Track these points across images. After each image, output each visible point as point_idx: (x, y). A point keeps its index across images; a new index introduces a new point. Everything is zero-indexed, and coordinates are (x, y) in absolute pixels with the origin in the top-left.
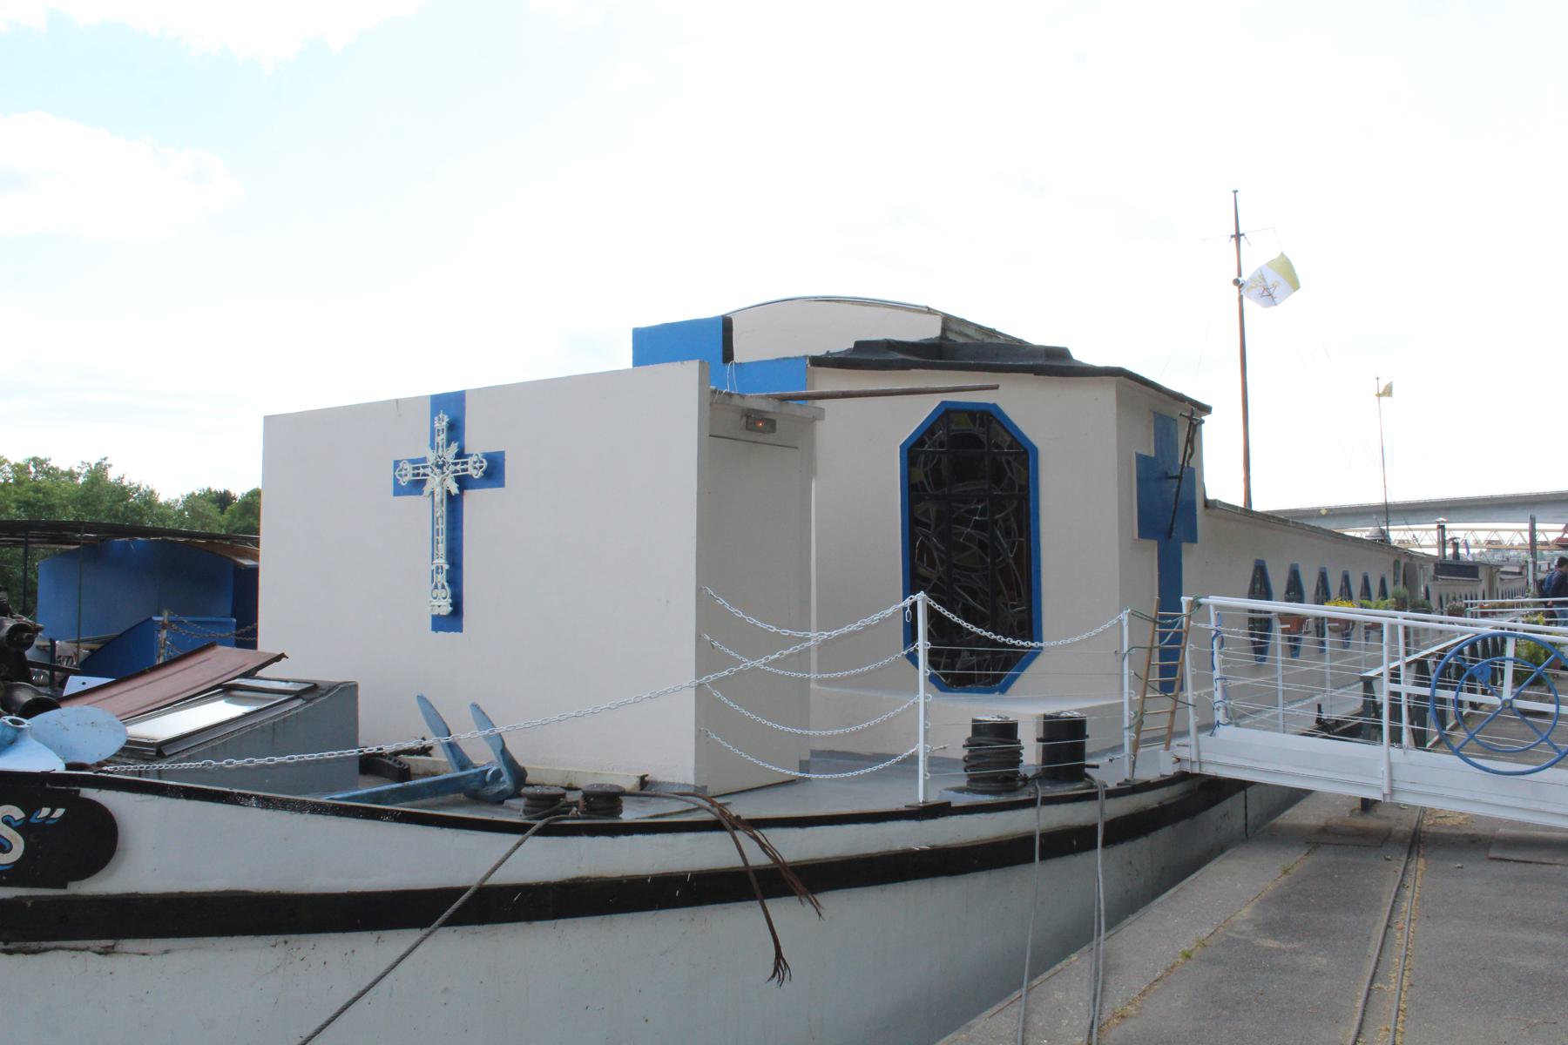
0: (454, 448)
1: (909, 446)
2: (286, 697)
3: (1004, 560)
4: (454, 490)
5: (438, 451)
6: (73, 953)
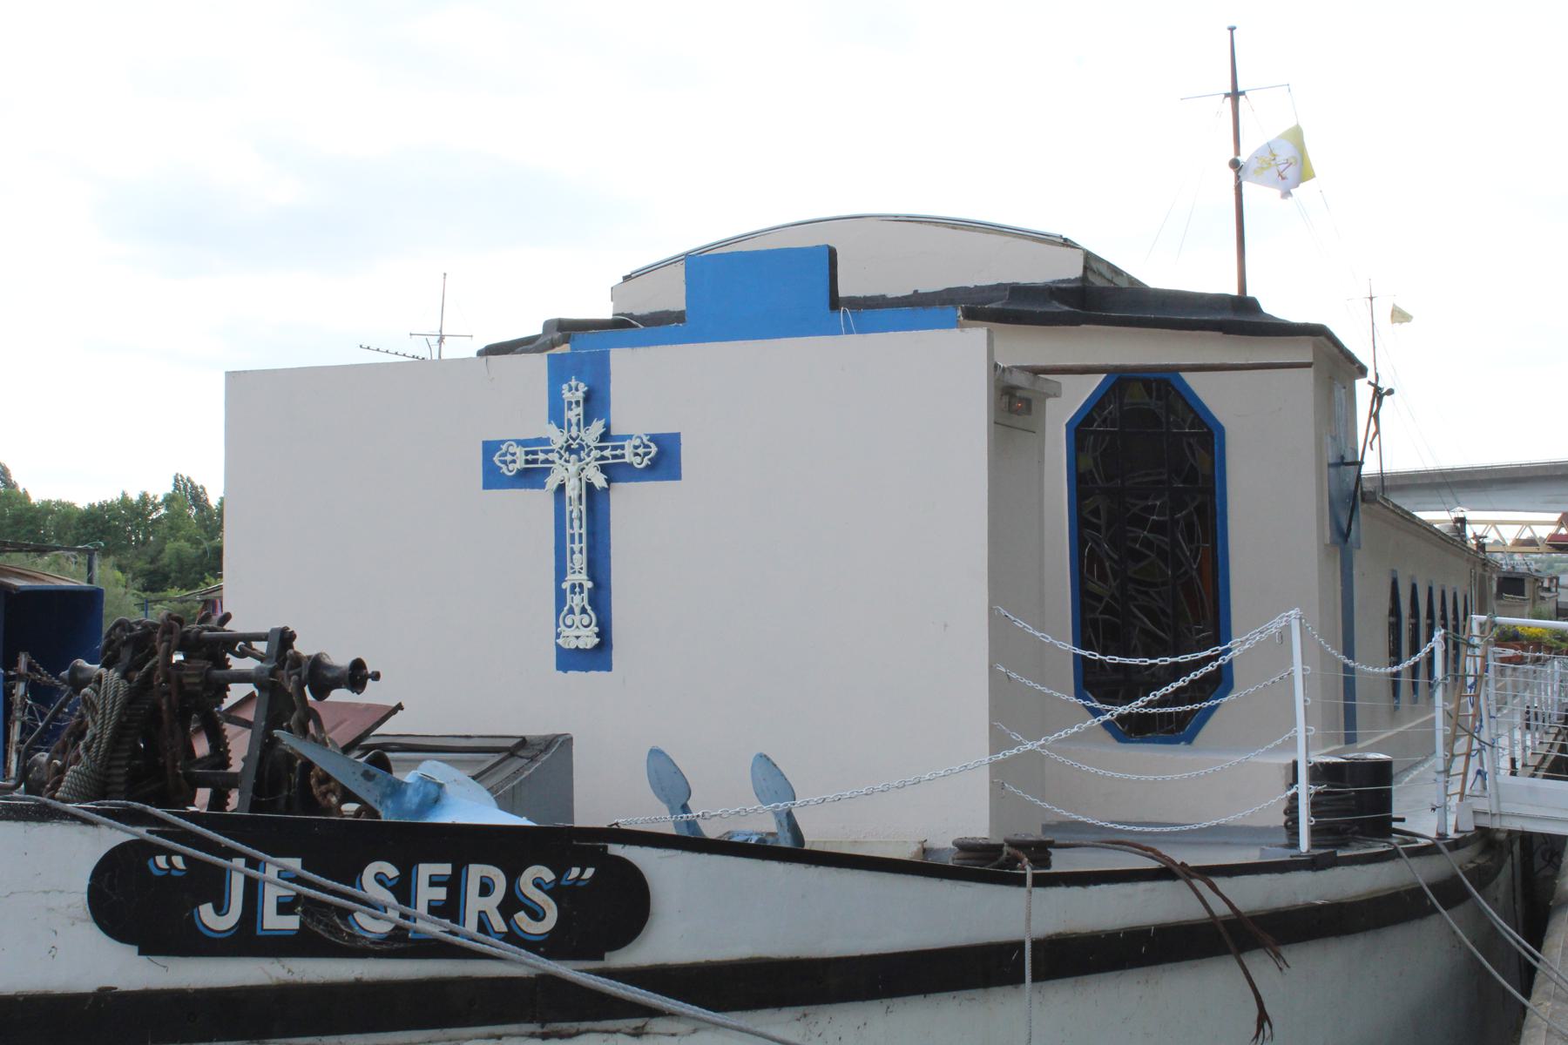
0: (597, 427)
1: (1075, 425)
2: (497, 757)
3: (1186, 572)
4: (599, 481)
5: (569, 431)
6: (605, 1036)
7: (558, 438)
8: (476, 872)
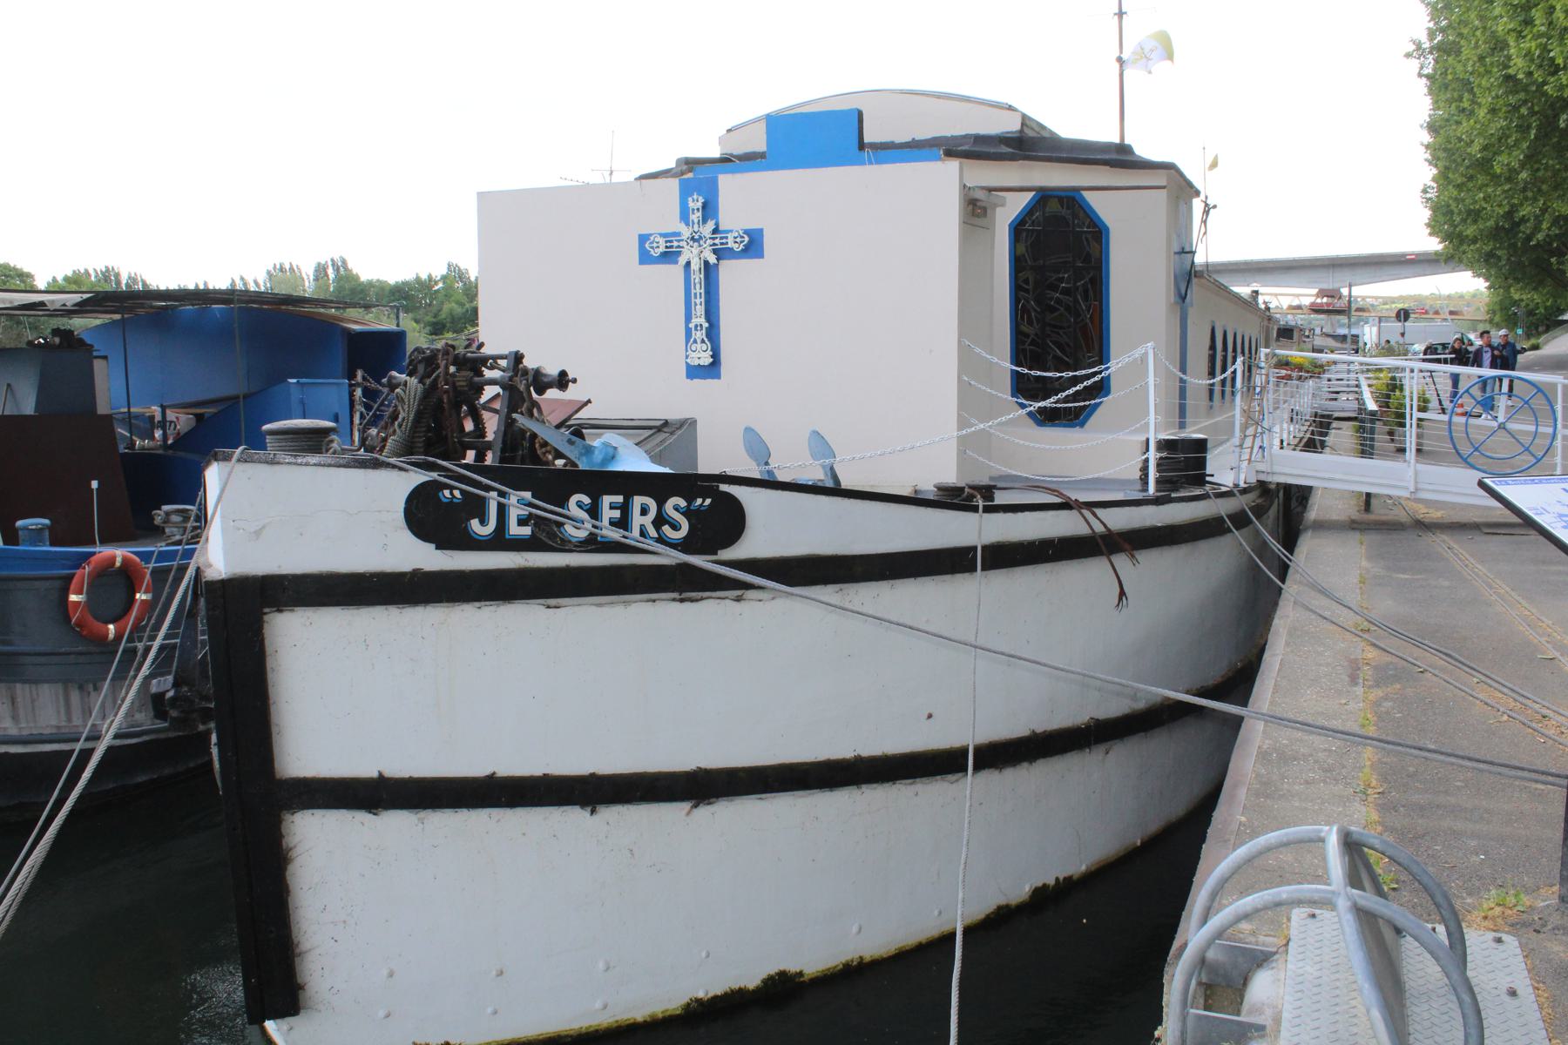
0: (711, 225)
2: (650, 432)
4: (712, 259)
6: (719, 601)
7: (686, 232)
8: (638, 501)
